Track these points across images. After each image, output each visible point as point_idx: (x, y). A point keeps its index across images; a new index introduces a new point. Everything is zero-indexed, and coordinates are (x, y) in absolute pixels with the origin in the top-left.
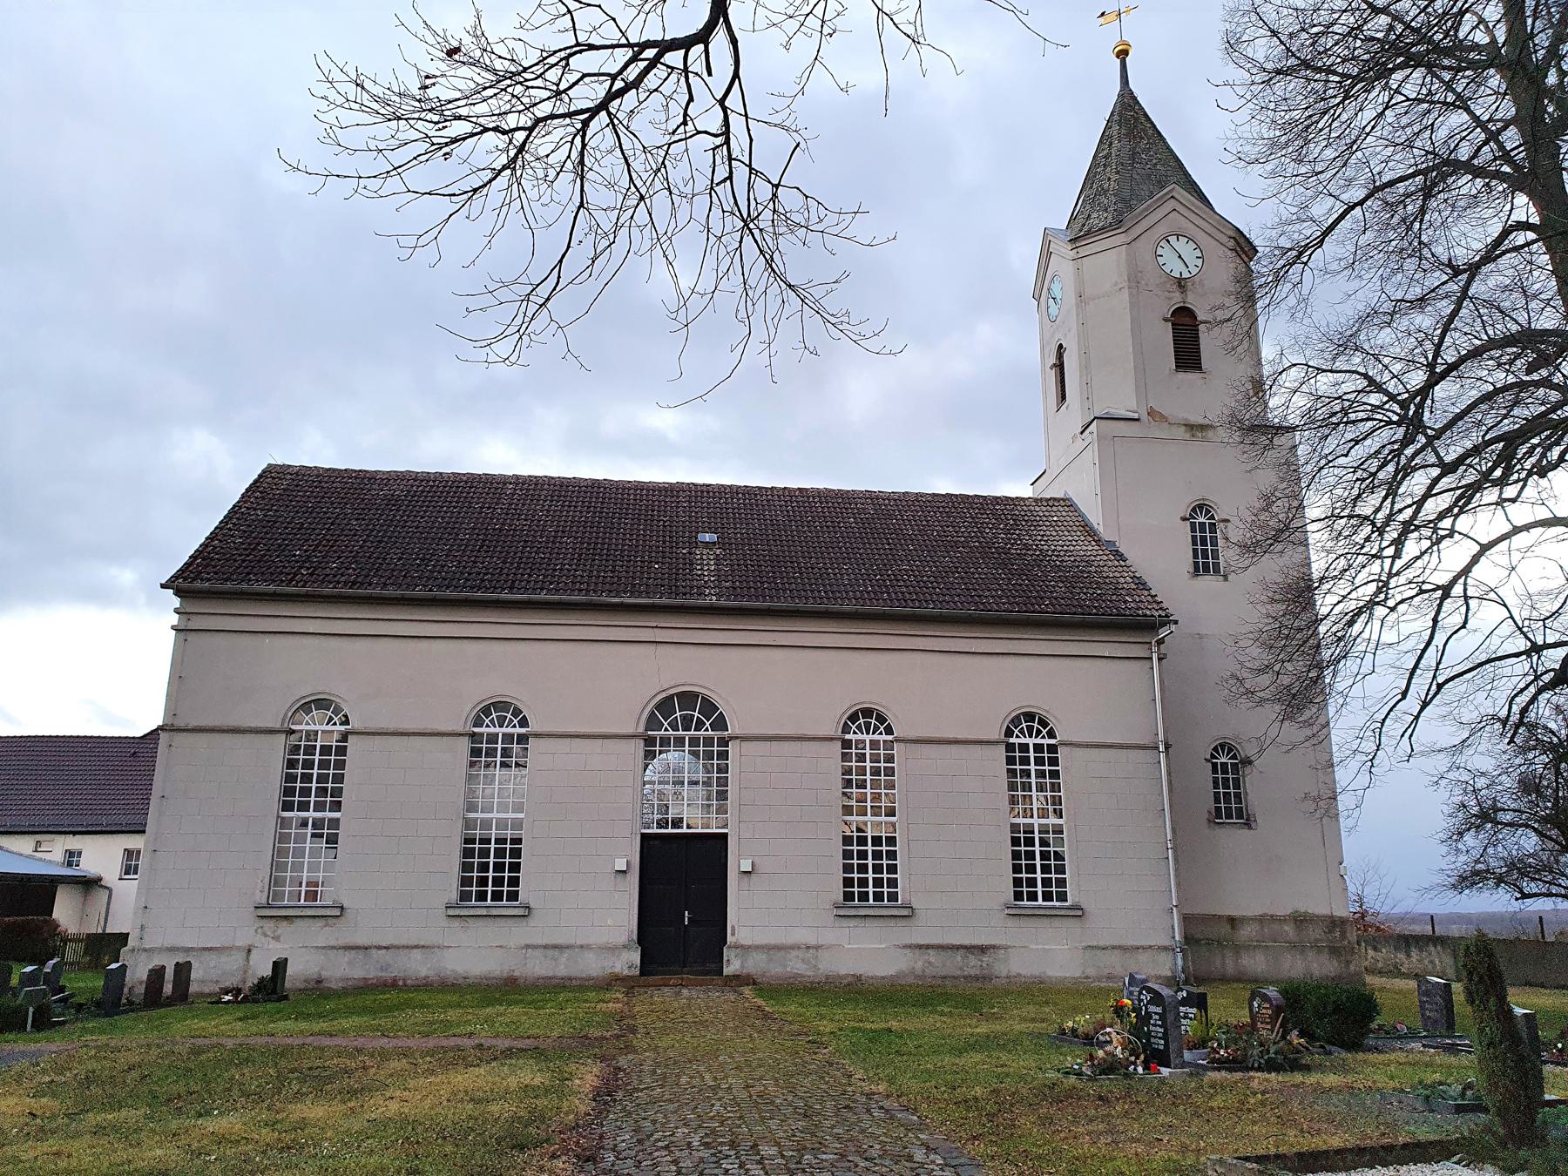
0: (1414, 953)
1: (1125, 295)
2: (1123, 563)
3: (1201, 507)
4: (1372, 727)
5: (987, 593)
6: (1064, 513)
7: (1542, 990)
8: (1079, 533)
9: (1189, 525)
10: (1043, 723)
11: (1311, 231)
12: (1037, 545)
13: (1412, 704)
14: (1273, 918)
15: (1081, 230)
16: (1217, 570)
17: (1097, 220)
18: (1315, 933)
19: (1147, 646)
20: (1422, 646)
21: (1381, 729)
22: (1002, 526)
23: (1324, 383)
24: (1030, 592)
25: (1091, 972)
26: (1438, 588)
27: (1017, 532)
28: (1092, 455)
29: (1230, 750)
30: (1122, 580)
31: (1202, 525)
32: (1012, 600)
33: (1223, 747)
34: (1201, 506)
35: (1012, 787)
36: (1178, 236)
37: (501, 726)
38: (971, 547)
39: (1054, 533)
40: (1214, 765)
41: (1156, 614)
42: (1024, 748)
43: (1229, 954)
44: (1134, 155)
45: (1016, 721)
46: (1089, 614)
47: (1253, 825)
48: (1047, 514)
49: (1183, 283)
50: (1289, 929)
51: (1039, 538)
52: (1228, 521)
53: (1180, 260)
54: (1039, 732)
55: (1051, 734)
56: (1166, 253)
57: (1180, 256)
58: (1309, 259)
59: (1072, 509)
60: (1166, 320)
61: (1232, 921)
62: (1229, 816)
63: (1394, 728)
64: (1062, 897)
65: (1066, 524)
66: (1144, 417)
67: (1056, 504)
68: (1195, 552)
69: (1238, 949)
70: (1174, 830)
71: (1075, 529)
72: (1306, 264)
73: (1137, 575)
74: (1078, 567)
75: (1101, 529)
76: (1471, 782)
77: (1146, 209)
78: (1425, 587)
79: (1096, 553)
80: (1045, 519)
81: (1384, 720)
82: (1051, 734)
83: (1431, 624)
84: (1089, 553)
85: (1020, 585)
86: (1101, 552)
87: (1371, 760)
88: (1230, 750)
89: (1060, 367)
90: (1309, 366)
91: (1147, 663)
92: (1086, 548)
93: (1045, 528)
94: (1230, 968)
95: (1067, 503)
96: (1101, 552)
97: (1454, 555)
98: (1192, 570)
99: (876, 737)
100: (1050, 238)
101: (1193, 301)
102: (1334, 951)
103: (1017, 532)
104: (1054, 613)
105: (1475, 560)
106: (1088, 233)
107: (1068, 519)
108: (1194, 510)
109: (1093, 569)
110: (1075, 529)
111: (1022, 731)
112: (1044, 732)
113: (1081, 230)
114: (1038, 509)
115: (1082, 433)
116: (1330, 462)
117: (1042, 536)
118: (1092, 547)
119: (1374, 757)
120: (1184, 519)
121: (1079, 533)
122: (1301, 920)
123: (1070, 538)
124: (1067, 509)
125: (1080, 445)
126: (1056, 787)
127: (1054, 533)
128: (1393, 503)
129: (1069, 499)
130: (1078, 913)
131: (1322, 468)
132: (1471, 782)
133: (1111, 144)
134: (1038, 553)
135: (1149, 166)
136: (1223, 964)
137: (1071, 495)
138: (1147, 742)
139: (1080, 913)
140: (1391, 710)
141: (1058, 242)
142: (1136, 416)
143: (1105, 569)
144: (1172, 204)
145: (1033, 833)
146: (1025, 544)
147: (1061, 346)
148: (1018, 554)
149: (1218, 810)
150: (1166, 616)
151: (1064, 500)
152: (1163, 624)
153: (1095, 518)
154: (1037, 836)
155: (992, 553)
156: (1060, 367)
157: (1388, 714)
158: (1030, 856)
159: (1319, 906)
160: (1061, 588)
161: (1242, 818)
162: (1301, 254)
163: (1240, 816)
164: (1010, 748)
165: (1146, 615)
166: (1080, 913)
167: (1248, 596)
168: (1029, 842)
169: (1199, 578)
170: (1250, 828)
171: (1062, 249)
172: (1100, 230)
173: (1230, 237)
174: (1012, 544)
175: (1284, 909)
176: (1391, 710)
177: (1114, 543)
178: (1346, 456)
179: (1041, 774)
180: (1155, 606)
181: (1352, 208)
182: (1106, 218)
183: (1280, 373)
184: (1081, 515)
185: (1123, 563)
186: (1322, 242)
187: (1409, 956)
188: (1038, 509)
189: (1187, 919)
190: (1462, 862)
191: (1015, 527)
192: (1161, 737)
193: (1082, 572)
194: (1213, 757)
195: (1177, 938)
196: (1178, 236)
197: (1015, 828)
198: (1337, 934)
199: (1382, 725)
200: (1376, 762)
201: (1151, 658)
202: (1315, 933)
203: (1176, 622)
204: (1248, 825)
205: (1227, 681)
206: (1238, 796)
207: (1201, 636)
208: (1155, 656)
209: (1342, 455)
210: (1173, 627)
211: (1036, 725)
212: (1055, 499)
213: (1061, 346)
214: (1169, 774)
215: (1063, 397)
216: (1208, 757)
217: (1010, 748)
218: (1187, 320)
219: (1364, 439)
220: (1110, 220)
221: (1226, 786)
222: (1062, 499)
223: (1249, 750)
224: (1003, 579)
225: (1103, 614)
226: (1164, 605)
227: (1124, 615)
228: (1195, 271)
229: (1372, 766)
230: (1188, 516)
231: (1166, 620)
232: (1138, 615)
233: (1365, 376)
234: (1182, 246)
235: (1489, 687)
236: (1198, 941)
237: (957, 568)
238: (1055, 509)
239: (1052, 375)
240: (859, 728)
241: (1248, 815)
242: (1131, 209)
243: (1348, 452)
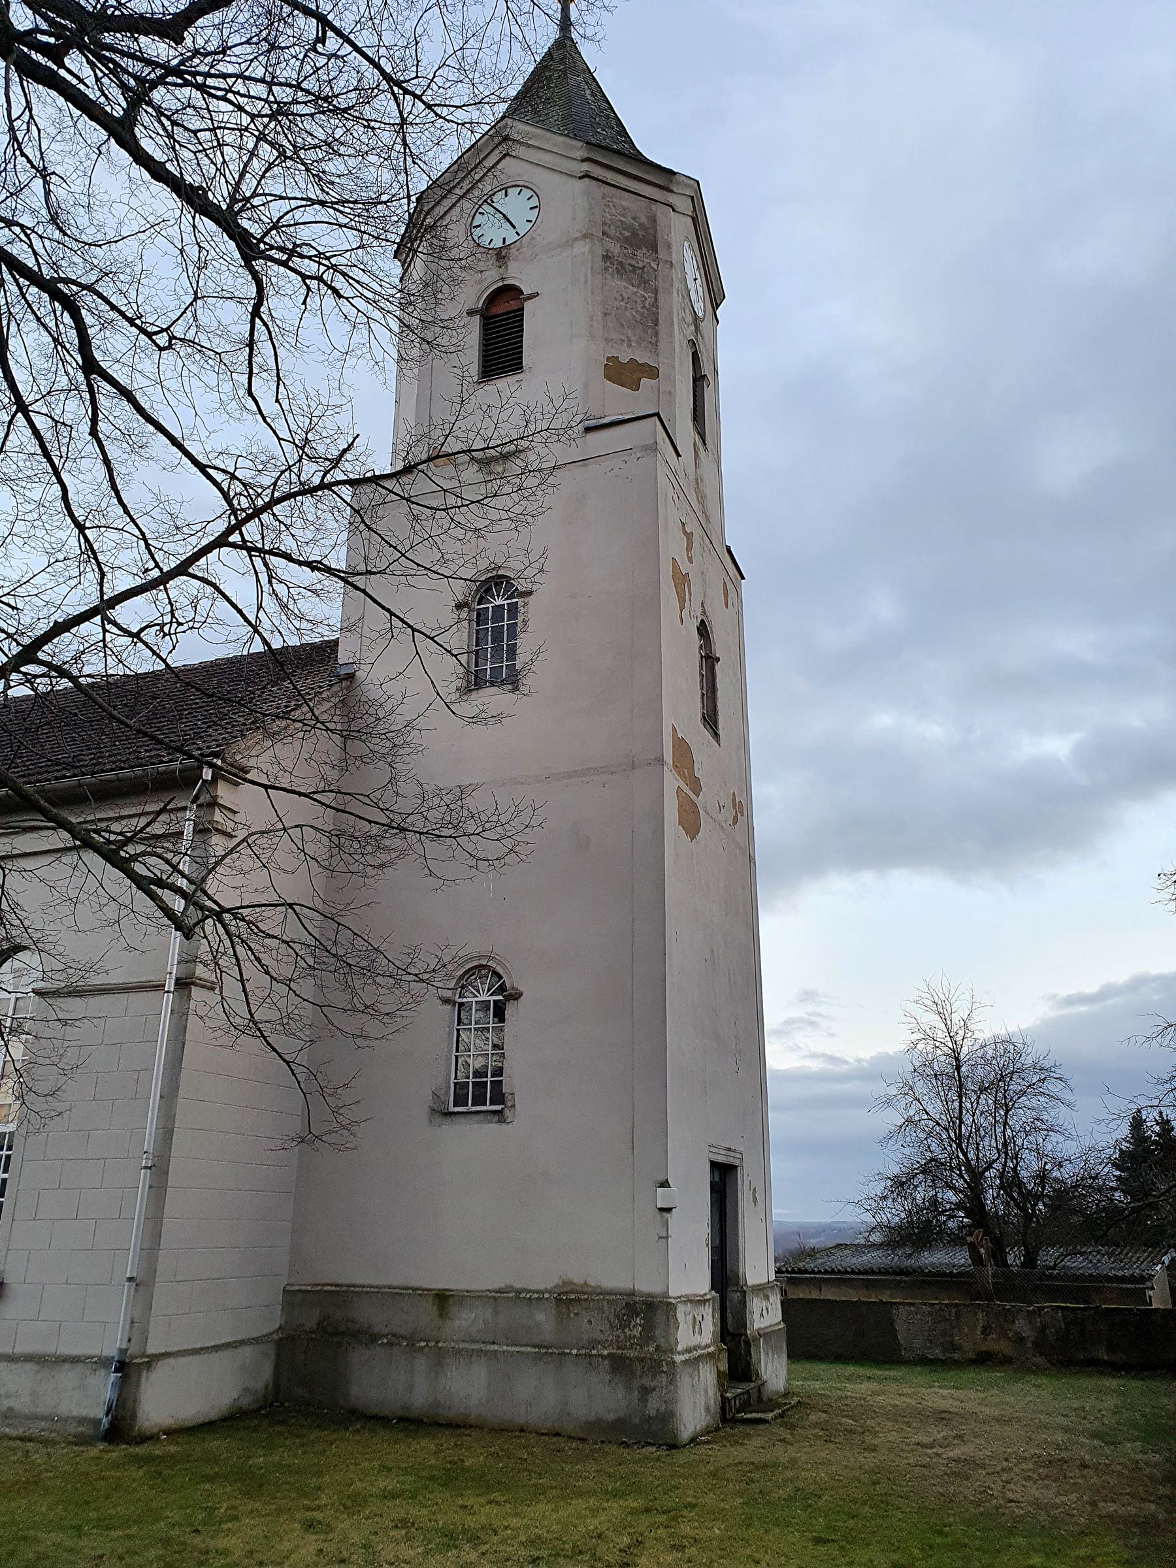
43: (421, 1364)
50: (544, 1319)
61: (443, 1299)
62: (479, 1100)
69: (439, 1357)
102: (620, 1365)
136: (410, 1388)
173: (583, 160)
198: (637, 1332)
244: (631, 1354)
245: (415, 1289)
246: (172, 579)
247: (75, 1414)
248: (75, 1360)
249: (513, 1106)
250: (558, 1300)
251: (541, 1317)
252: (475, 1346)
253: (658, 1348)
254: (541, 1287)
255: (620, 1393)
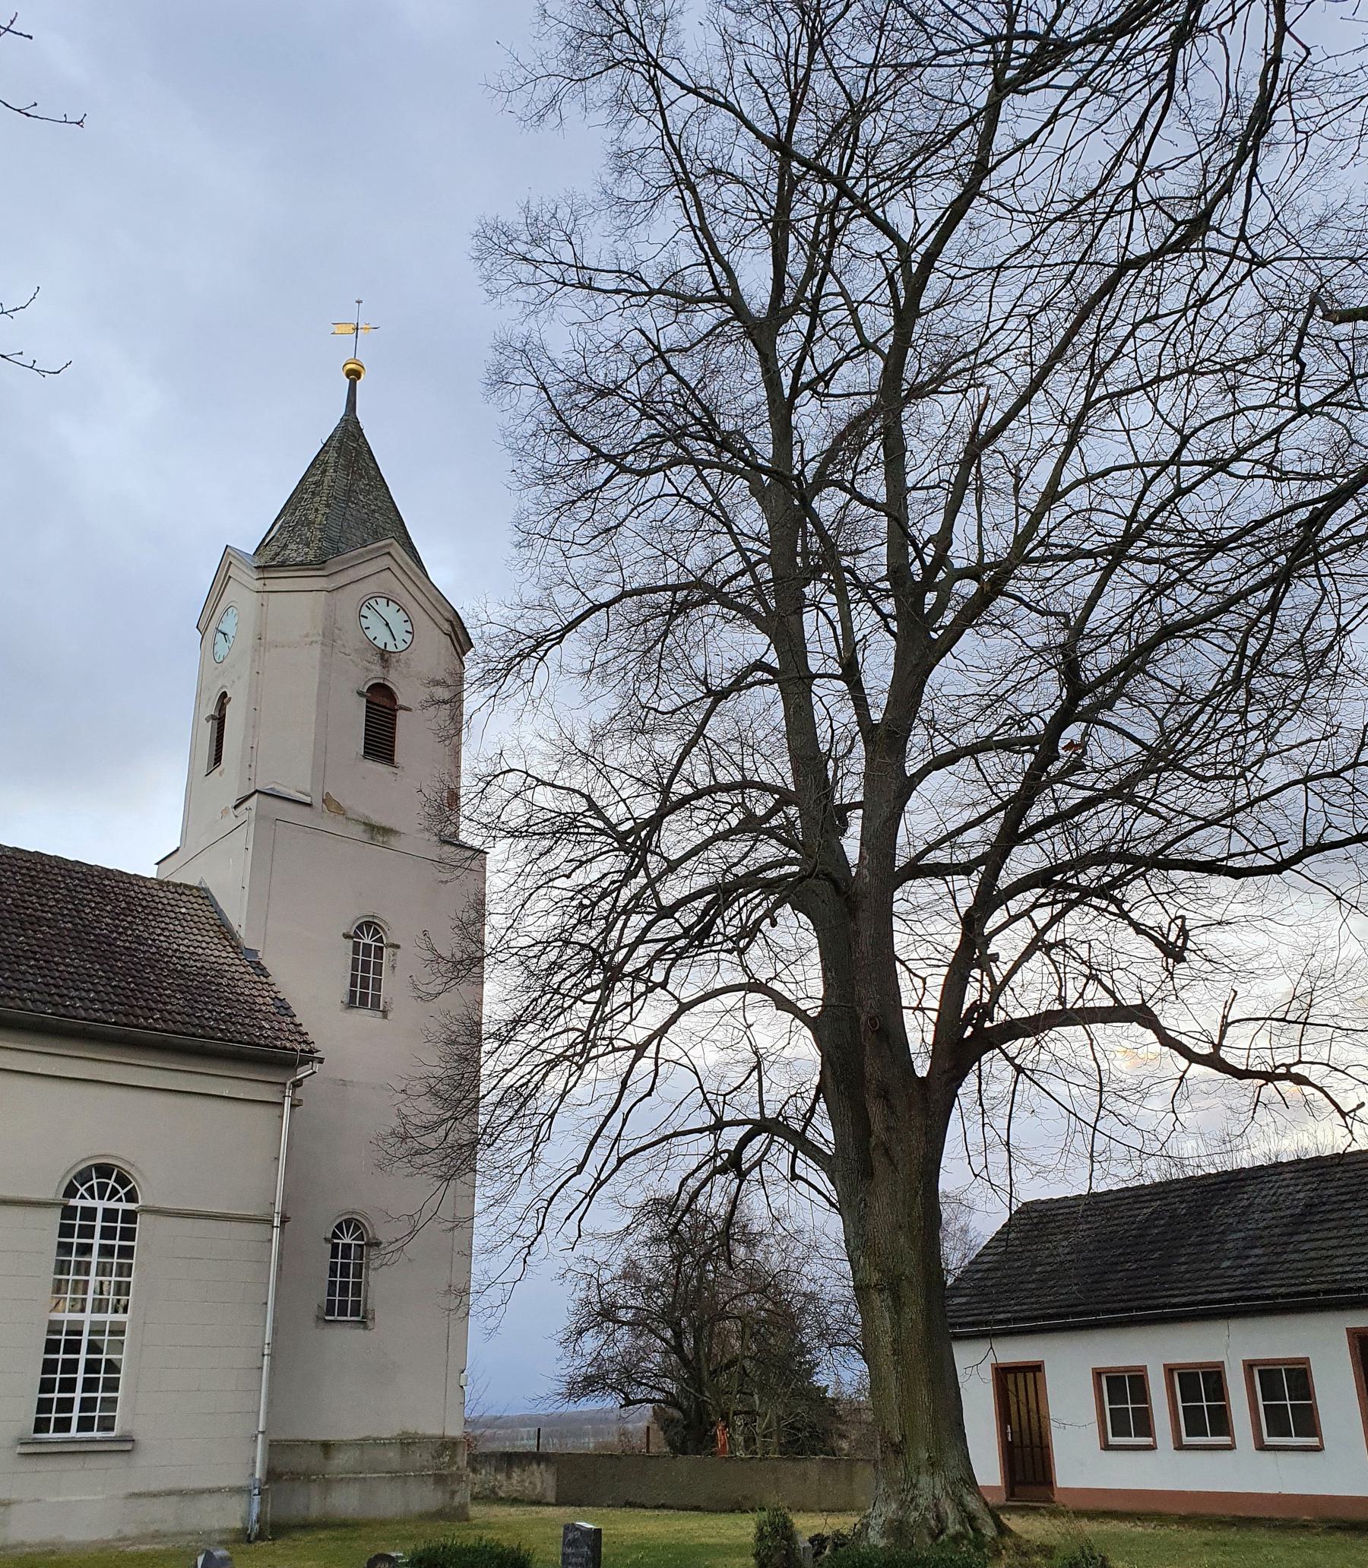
0: (516, 1474)
1: (316, 651)
2: (265, 980)
3: (369, 925)
4: (537, 1207)
5: (73, 993)
6: (196, 906)
7: (643, 1511)
8: (212, 934)
9: (351, 944)
10: (123, 1180)
11: (551, 622)
12: (154, 940)
13: (585, 1181)
14: (377, 1442)
15: (273, 559)
16: (376, 1006)
17: (294, 553)
18: (421, 1457)
19: (279, 1087)
20: (606, 1113)
21: (547, 1209)
22: (108, 908)
23: (544, 797)
24: (137, 999)
25: (131, 1530)
26: (632, 1047)
27: (129, 919)
28: (244, 838)
29: (357, 1228)
30: (260, 1000)
31: (367, 946)
32: (109, 1007)
33: (350, 1224)
34: (369, 924)
35: (62, 1267)
36: (388, 600)
37: (101, 1197)
38: (59, 929)
39: (179, 929)
40: (335, 1247)
41: (298, 1047)
42: (89, 1213)
44: (349, 493)
45: (83, 1176)
46: (212, 1038)
47: (370, 1324)
48: (173, 902)
49: (387, 656)
50: (393, 1455)
51: (159, 931)
52: (398, 947)
53: (386, 628)
54: (115, 1192)
55: (131, 1197)
56: (372, 621)
57: (387, 624)
58: (545, 655)
59: (207, 902)
60: (360, 694)
61: (326, 1447)
62: (343, 1312)
63: (560, 1208)
64: (107, 1424)
65: (196, 919)
66: (317, 802)
67: (187, 892)
68: (354, 977)
69: (327, 1484)
70: (275, 1331)
71: (208, 927)
72: (541, 659)
73: (280, 996)
74: (206, 975)
75: (242, 933)
76: (596, 1275)
77: (356, 557)
78: (618, 1044)
79: (231, 961)
80: (169, 908)
81: (552, 1198)
82: (131, 1197)
83: (619, 1087)
84: (223, 961)
85: (123, 989)
86: (237, 962)
87: (529, 1247)
88: (357, 1228)
89: (219, 721)
90: (529, 775)
91: (276, 1111)
92: (218, 953)
93: (167, 920)
94: (315, 1511)
95: (203, 895)
96: (237, 962)
97: (653, 1013)
98: (346, 999)
99: (112, 1205)
100: (231, 559)
101: (396, 681)
102: (440, 1479)
103: (129, 919)
104: (165, 1031)
105: (673, 1019)
106: (282, 565)
107: (200, 913)
108: (359, 928)
109: (224, 981)
110: (208, 927)
111: (90, 1190)
112: (122, 1192)
113: (273, 559)
114: (162, 894)
115: (236, 807)
116: (550, 880)
117: (163, 929)
118: (227, 955)
119: (533, 1243)
120: (346, 936)
121: (212, 934)
122: (407, 1442)
123: (200, 938)
124: (201, 901)
125: (230, 822)
126: (125, 1270)
127: (179, 929)
128: (741, 919)
129: (206, 890)
130: (127, 1445)
131: (541, 886)
132: (596, 1275)
133: (324, 471)
134: (154, 950)
135: (365, 511)
136: (308, 1507)
137: (209, 884)
138: (257, 1213)
139: (128, 1446)
140: (562, 1186)
141: (241, 566)
142: (308, 800)
143: (240, 983)
144: (386, 561)
145: (80, 1333)
146: (138, 936)
147: (224, 695)
148: (127, 948)
149: (331, 1303)
150: (311, 1052)
151: (198, 889)
152: (305, 1062)
153: (236, 916)
154: (85, 1339)
155: (90, 941)
156: (219, 721)
157: (558, 1190)
158: (71, 1366)
159: (430, 1426)
160: (178, 1002)
161: (358, 1315)
162: (539, 644)
163: (355, 1312)
164: (68, 1212)
165: (285, 1048)
166: (128, 1446)
167: (426, 1033)
168: (73, 1347)
169: (355, 1011)
170: (366, 1328)
171: (245, 577)
172: (302, 564)
173: (447, 620)
174: (120, 934)
175: (390, 1429)
176: (562, 1186)
177: (255, 952)
178: (568, 876)
179: (107, 1251)
180: (297, 1037)
181: (595, 608)
182: (306, 554)
183: (496, 776)
184: (219, 912)
185: (265, 980)
186: (562, 637)
187: (509, 1477)
188: (162, 894)
189: (275, 1447)
190: (579, 1366)
191: (128, 912)
192: (278, 1208)
193: (210, 982)
194: (335, 1235)
195: (257, 1476)
196: (388, 600)
197: (54, 1327)
198: (446, 1459)
199: (549, 1204)
200: (533, 1249)
201: (282, 1104)
202: (421, 1457)
203: (321, 1061)
204: (363, 1324)
205: (384, 1140)
206: (357, 1286)
207: (344, 1083)
208: (287, 1102)
209: (564, 876)
210: (317, 1067)
211: (112, 1182)
212: (186, 886)
213: (224, 695)
214: (280, 1255)
215: (218, 759)
216: (329, 1235)
217: (68, 1212)
218: (385, 702)
219: (590, 861)
220: (311, 557)
221: (345, 1273)
222: (196, 888)
223: (383, 1233)
224: (100, 977)
225: (230, 1041)
226: (310, 1038)
227: (258, 1045)
228: (402, 646)
229: (529, 1253)
230: (352, 934)
231: (309, 1056)
232: (276, 1047)
233: (588, 798)
234: (390, 612)
235: (663, 1166)
236: (280, 1476)
237: (35, 953)
238: (184, 898)
239: (207, 729)
240: (90, 1190)
241: (365, 1311)
242: (338, 552)
243: (571, 874)
244: (445, 1473)
245: (305, 1441)
246: (936, 1031)
247: (217, 1527)
248: (211, 1491)
249: (373, 1318)
250: (402, 1444)
251: (391, 1454)
252: (351, 1475)
253: (458, 1468)
254: (389, 1436)
255: (440, 1495)
